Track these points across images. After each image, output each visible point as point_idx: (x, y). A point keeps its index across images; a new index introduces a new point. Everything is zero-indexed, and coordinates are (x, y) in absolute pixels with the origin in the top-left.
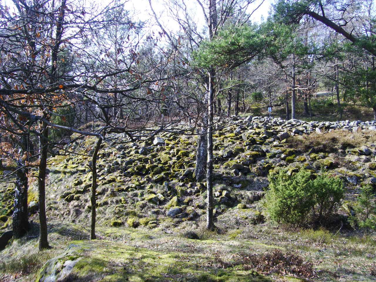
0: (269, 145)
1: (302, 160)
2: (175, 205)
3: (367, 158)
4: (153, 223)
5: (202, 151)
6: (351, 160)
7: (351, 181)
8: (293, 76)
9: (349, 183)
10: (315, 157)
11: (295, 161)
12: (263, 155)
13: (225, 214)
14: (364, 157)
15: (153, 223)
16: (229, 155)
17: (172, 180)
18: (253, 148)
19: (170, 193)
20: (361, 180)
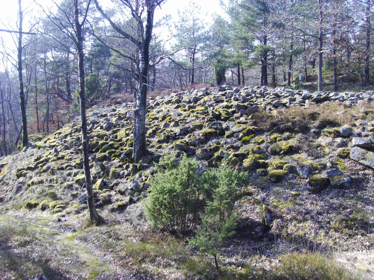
0: (234, 121)
1: (259, 141)
2: (97, 189)
3: (344, 142)
4: (59, 207)
5: (137, 129)
6: (322, 144)
7: (301, 173)
8: (319, 36)
9: (298, 175)
10: (275, 138)
11: (251, 143)
12: (221, 133)
13: (139, 203)
14: (339, 140)
15: (59, 207)
16: (182, 133)
17: (114, 160)
18: (212, 125)
19: (103, 174)
20: (317, 171)
